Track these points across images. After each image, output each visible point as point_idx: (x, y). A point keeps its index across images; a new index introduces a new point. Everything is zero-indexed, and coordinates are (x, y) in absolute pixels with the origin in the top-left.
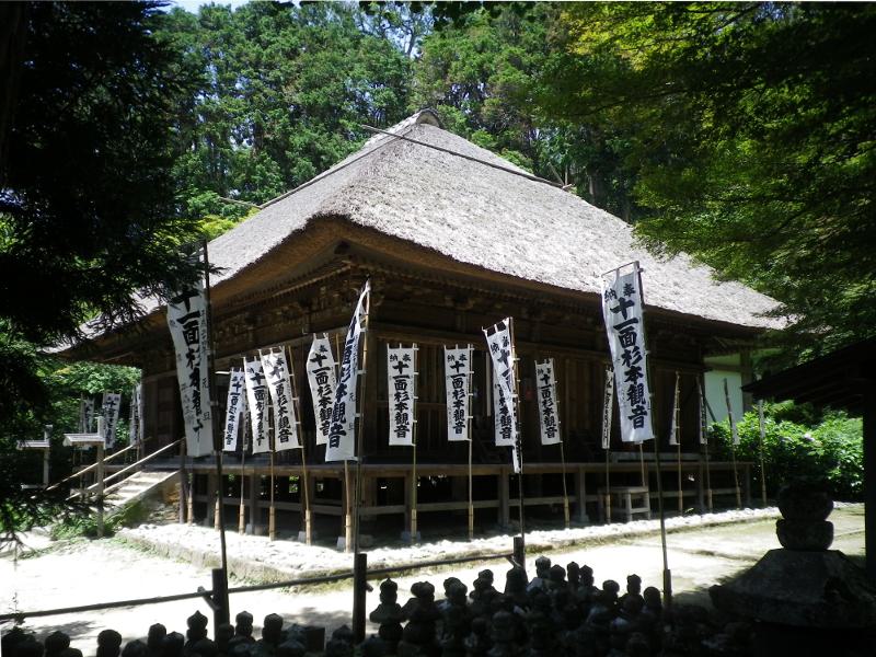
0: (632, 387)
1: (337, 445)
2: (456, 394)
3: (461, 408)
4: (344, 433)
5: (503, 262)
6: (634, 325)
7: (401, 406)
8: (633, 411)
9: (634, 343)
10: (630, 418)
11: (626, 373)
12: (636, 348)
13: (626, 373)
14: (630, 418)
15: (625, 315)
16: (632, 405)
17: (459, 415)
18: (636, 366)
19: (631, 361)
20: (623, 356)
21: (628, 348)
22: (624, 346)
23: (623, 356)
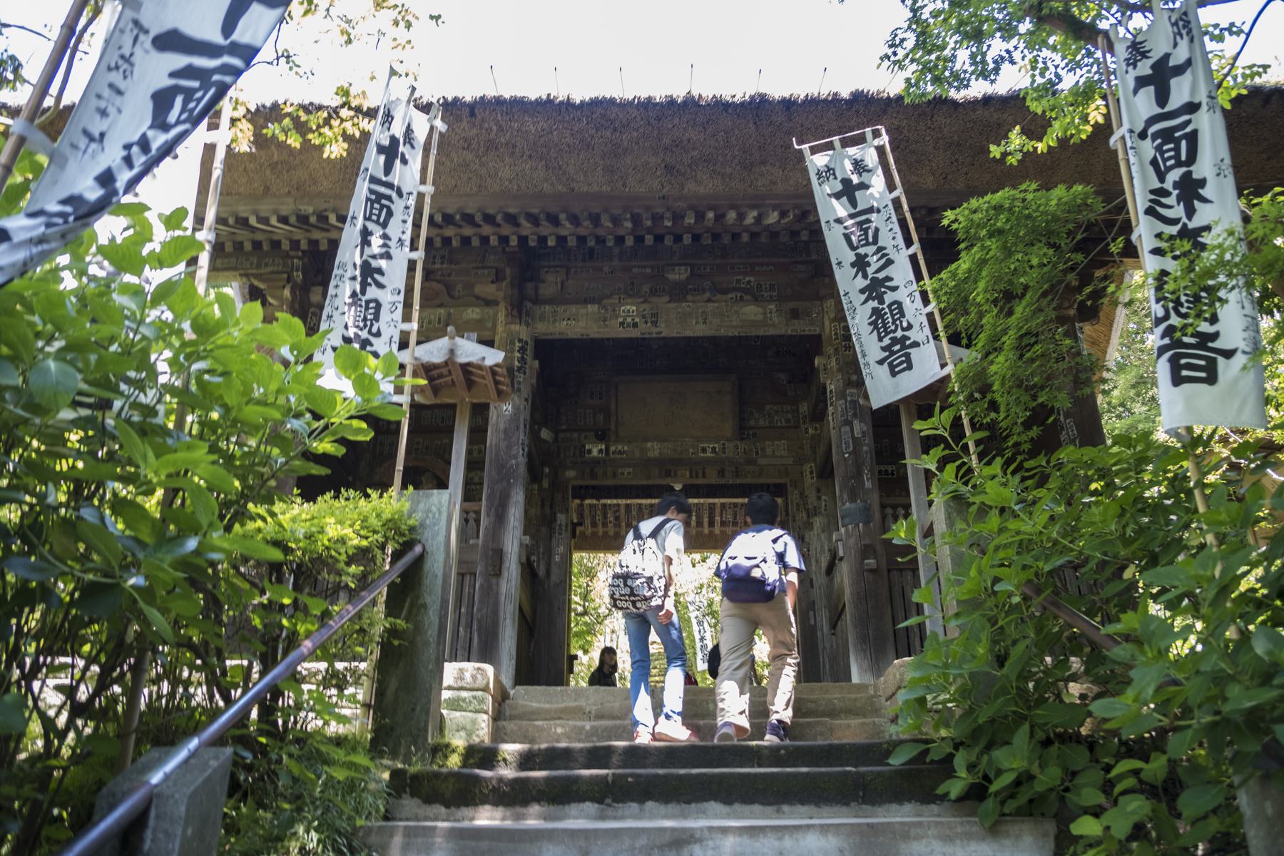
0: (875, 311)
7: (876, 289)
8: (883, 349)
14: (881, 362)
16: (881, 339)
18: (881, 275)
19: (870, 270)
21: (862, 251)
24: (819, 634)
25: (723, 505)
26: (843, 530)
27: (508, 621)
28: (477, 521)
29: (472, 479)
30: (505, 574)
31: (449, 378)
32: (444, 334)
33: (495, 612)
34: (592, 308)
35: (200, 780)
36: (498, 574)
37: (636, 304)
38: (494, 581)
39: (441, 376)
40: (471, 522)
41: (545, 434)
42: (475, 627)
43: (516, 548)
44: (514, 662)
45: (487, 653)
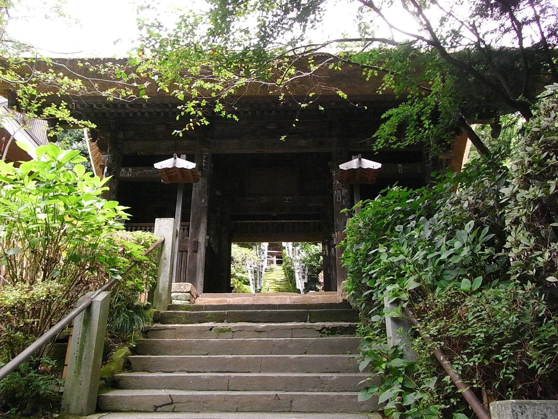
24: (331, 277)
25: (299, 223)
26: (336, 233)
27: (201, 270)
28: (188, 230)
29: (541, 393)
30: (199, 251)
31: (175, 173)
32: (171, 156)
33: (195, 266)
34: (236, 141)
35: (254, 152)
36: (196, 251)
37: (241, 155)
38: (195, 254)
39: (171, 173)
40: (186, 230)
41: (218, 193)
42: (187, 272)
43: (204, 240)
44: (203, 286)
45: (193, 280)
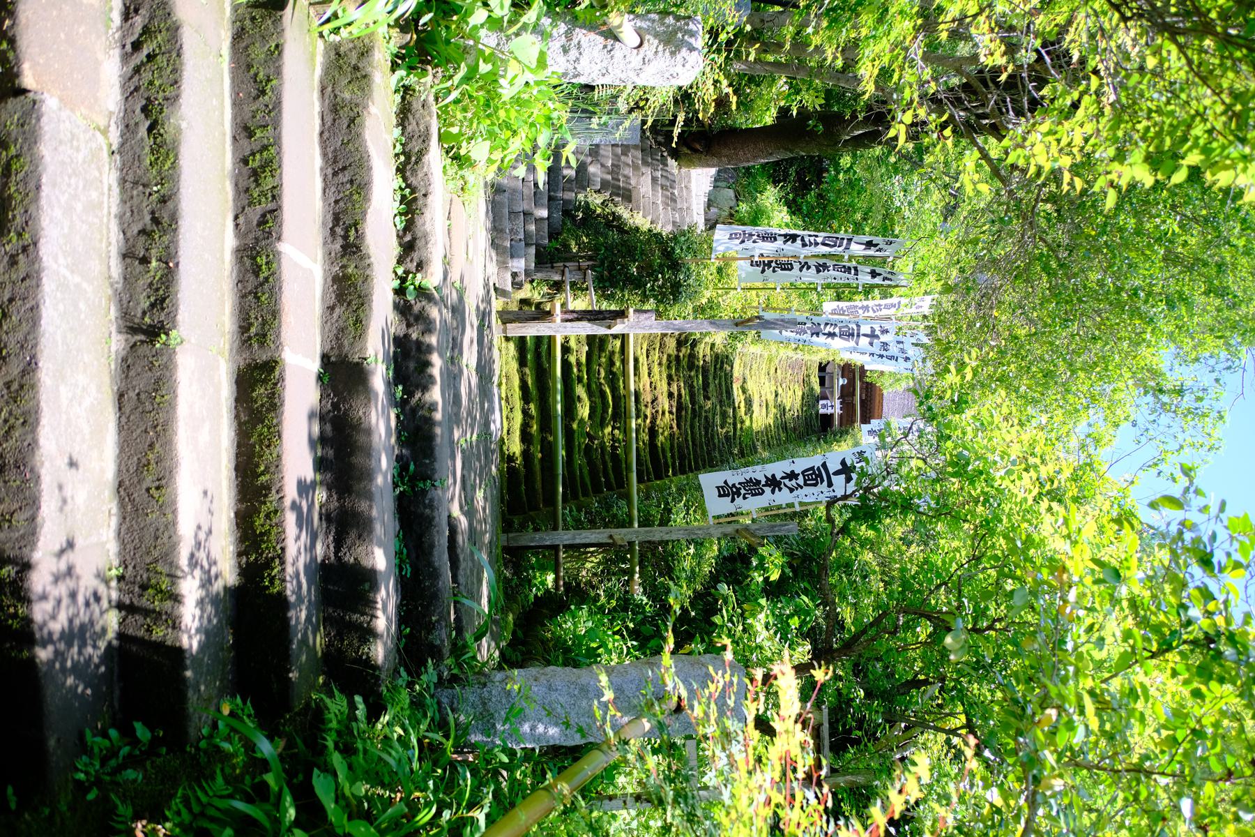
0: (758, 482)
1: (720, 496)
2: (792, 476)
3: (768, 490)
4: (733, 501)
5: (46, 128)
6: (825, 483)
9: (806, 484)
10: (726, 482)
11: (773, 476)
12: (817, 244)
13: (773, 476)
14: (726, 482)
15: (837, 473)
17: (754, 488)
19: (787, 481)
20: (793, 472)
21: (801, 477)
22: (803, 472)
23: (793, 472)
